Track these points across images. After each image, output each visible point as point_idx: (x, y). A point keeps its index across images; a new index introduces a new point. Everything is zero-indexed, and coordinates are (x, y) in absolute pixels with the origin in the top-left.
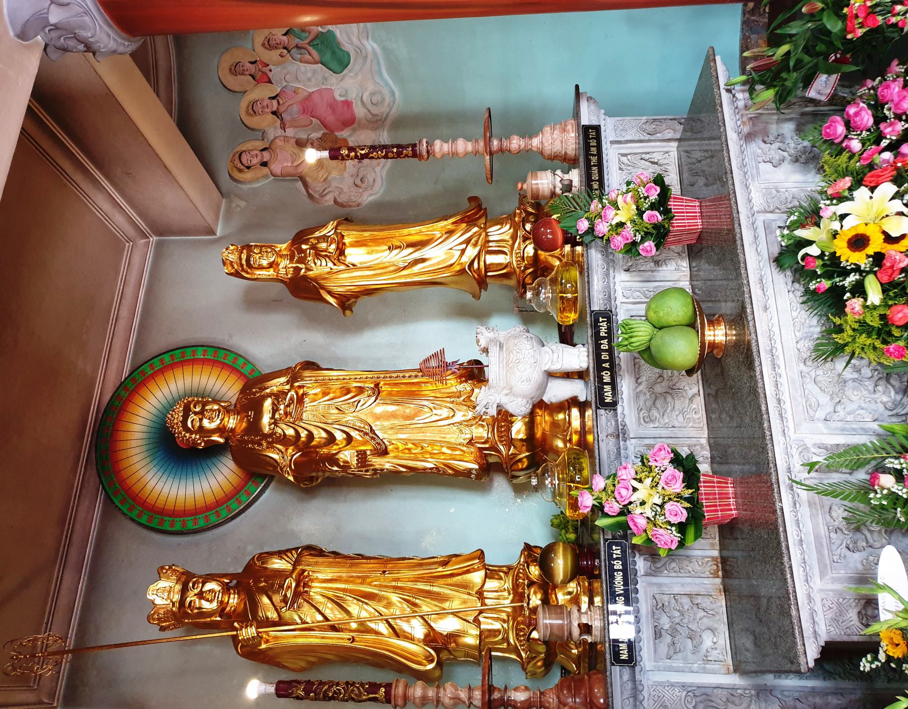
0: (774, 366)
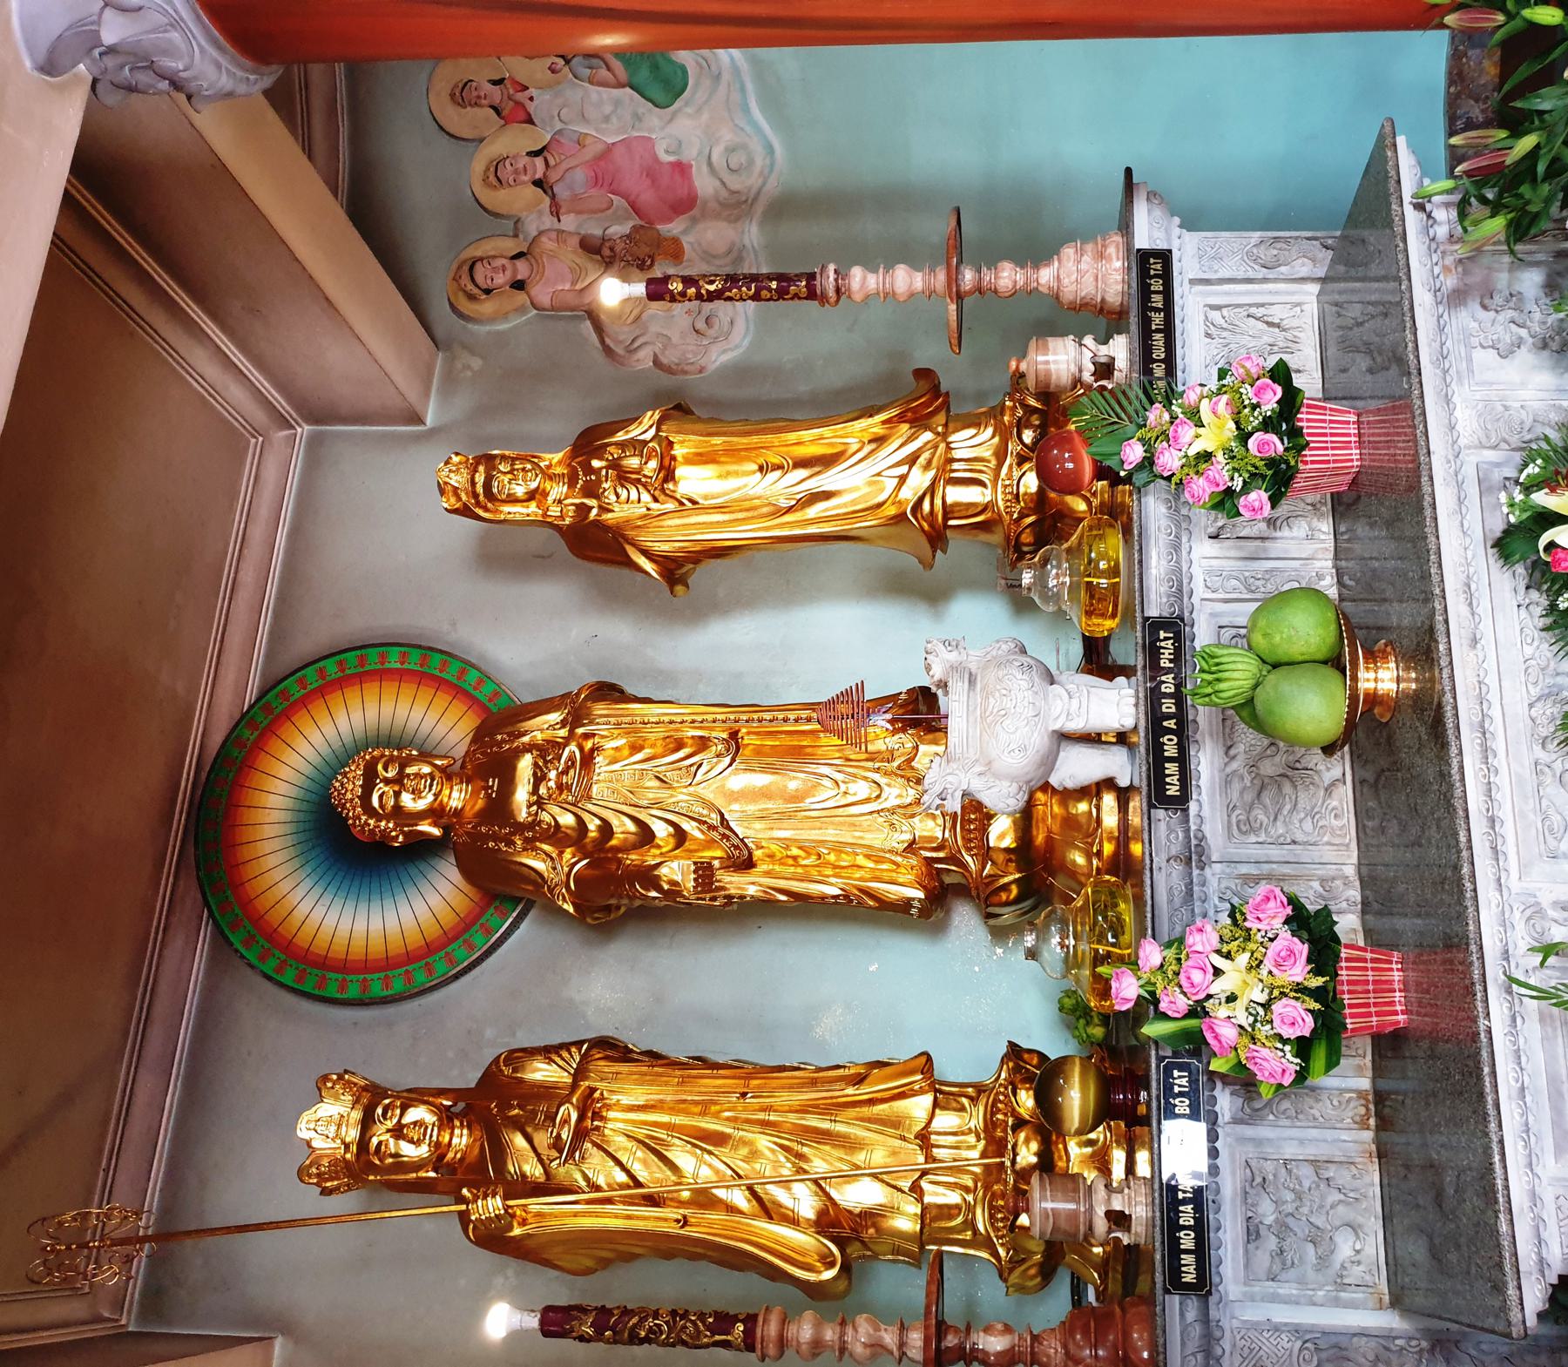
0: (1486, 752)
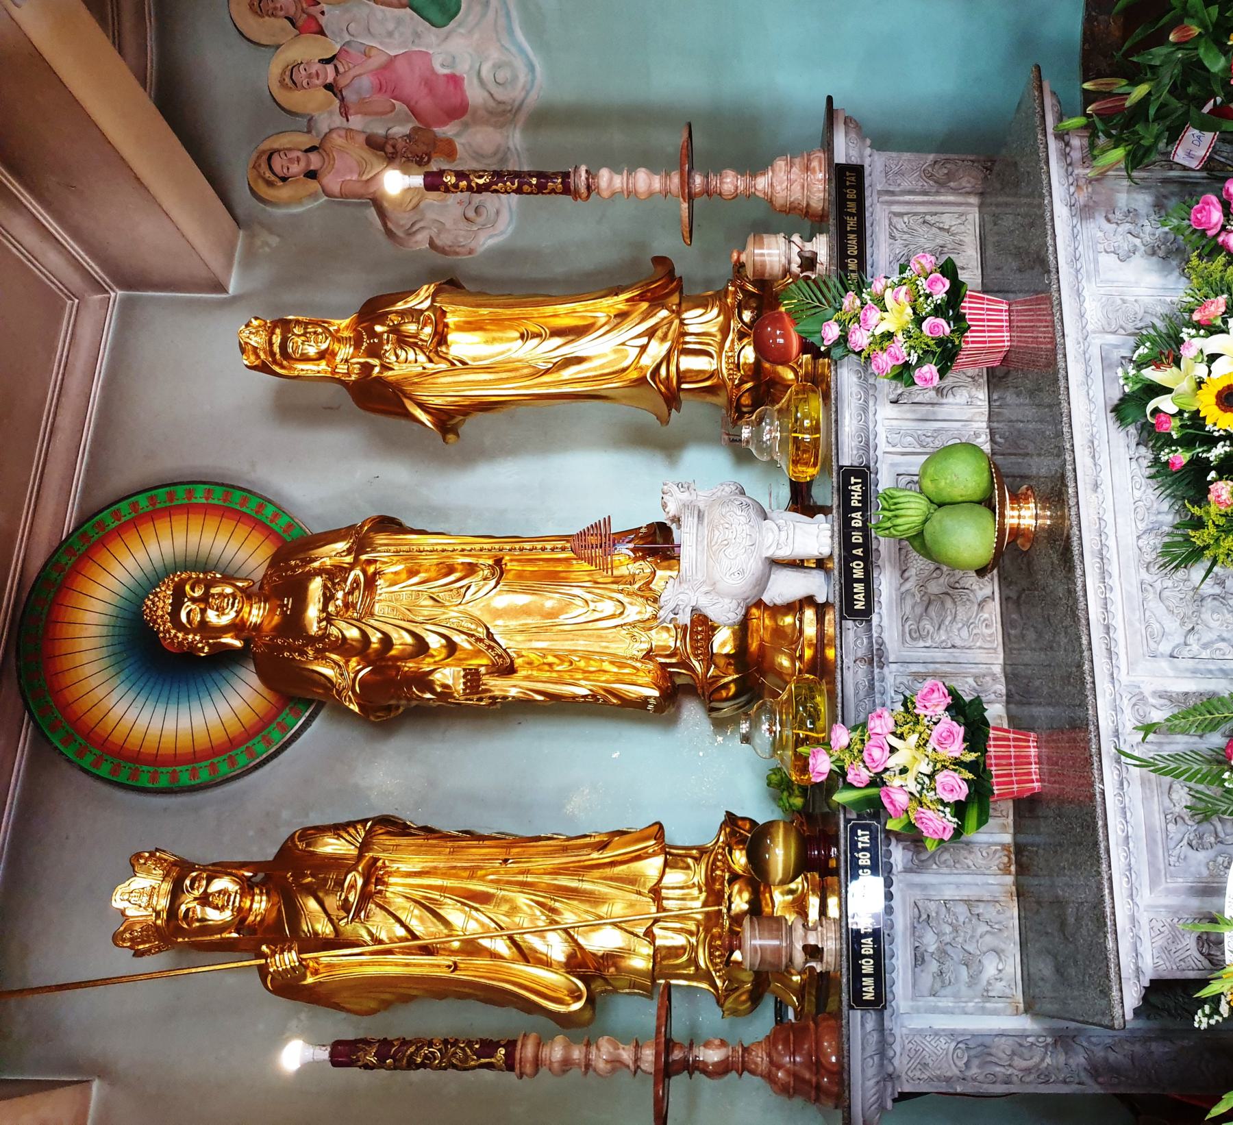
0: (1104, 574)
